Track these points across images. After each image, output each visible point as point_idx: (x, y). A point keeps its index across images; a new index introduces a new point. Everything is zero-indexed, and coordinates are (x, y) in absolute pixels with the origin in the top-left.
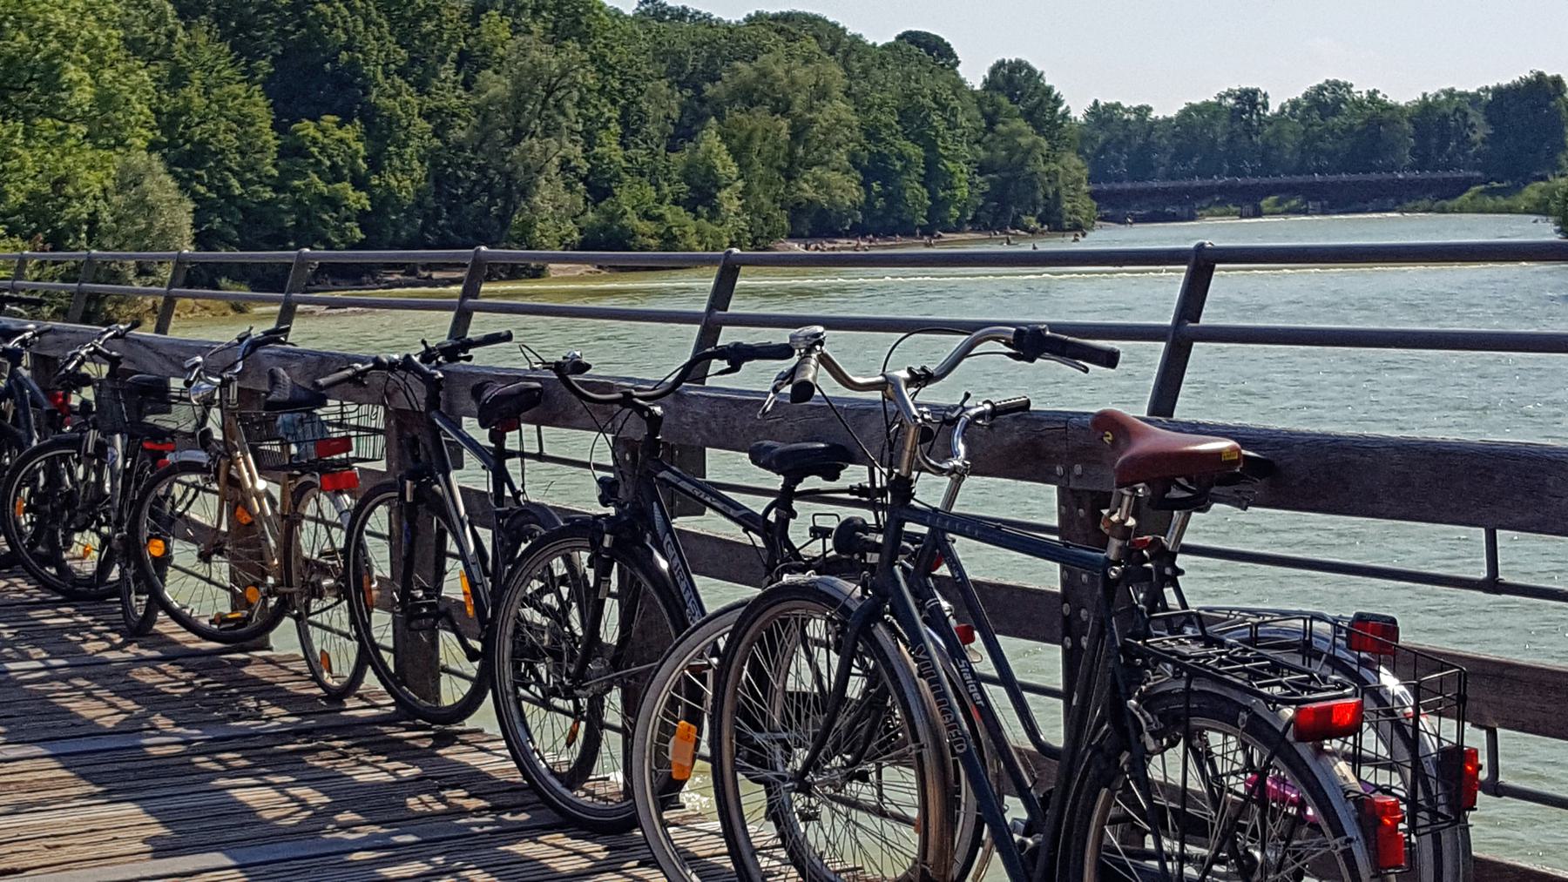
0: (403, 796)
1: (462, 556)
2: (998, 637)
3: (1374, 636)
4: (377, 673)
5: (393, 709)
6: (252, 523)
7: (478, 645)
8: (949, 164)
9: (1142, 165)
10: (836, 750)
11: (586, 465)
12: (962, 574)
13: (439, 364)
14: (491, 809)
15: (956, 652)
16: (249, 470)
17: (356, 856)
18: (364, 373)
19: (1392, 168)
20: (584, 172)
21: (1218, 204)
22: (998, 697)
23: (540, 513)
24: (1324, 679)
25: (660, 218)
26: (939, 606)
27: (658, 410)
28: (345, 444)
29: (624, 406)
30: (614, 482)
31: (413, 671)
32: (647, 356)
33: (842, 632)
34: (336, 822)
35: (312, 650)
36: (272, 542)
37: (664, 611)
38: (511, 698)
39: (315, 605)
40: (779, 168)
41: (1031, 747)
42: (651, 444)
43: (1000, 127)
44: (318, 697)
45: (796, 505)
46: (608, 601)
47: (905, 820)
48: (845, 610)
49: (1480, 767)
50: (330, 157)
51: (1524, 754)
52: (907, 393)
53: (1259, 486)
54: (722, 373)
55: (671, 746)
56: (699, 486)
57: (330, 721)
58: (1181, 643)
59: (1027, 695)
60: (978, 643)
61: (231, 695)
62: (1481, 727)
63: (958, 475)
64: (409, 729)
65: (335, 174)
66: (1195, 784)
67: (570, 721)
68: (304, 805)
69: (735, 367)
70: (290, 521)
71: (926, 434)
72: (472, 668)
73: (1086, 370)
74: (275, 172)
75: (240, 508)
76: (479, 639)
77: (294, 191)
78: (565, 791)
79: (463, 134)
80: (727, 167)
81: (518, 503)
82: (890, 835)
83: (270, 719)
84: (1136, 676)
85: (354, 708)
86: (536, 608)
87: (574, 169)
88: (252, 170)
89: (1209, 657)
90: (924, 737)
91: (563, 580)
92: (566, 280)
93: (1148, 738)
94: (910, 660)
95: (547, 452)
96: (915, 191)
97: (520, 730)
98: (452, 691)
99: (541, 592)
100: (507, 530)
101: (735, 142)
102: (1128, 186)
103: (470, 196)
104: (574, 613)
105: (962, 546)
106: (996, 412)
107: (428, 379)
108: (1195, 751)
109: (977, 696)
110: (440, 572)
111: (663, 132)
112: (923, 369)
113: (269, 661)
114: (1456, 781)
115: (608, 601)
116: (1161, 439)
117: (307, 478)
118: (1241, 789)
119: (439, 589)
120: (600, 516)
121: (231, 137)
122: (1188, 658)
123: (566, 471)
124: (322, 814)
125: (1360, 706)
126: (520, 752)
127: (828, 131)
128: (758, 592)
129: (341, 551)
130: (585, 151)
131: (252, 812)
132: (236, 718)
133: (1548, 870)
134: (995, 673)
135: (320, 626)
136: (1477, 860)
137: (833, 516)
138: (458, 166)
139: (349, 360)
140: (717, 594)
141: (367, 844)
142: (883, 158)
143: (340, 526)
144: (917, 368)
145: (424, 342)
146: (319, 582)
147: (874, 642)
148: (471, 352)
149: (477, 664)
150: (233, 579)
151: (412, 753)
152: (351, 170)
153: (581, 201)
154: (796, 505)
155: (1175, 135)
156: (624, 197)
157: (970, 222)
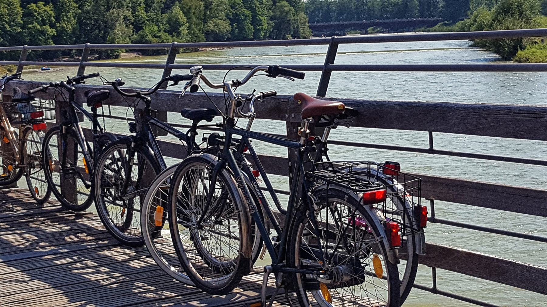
0: (64, 236)
1: (83, 152)
2: (267, 174)
3: (392, 169)
4: (55, 194)
5: (61, 206)
6: (9, 143)
7: (90, 183)
8: (261, 17)
9: (327, 15)
10: (211, 215)
11: (125, 119)
12: (254, 152)
13: (73, 84)
14: (95, 240)
15: (252, 179)
16: (8, 124)
17: (46, 257)
18: (46, 88)
19: (412, 17)
20: (132, 21)
21: (353, 30)
22: (267, 195)
23: (109, 136)
24: (373, 183)
25: (159, 37)
26: (246, 164)
27: (149, 98)
28: (41, 114)
29: (137, 98)
30: (135, 124)
31: (68, 193)
32: (144, 78)
33: (211, 173)
34: (39, 246)
35: (32, 186)
36: (17, 150)
37: (154, 170)
38: (100, 200)
39: (33, 171)
40: (201, 19)
41: (279, 212)
42: (147, 111)
43: (277, 4)
44: (34, 203)
45: (197, 130)
46: (134, 166)
47: (236, 238)
48: (213, 165)
49: (427, 213)
50: (41, 16)
51: (444, 208)
52: (232, 89)
53: (353, 119)
54: (172, 85)
55: (155, 214)
56: (164, 125)
57: (37, 211)
58: (326, 173)
59: (266, 187)
60: (260, 177)
61: (3, 203)
62: (429, 200)
63: (251, 118)
64: (66, 213)
65: (43, 23)
66: (331, 221)
67: (122, 208)
68: (28, 240)
69: (176, 83)
70: (22, 142)
71: (239, 104)
72: (88, 192)
73: (294, 80)
74: (22, 22)
75: (5, 138)
76: (90, 181)
77: (29, 29)
78: (121, 233)
79: (89, 8)
80: (182, 18)
81: (102, 133)
82: (232, 244)
83: (17, 211)
84: (310, 184)
85: (47, 206)
86: (109, 169)
87: (129, 20)
88: (13, 21)
89: (334, 177)
90: (240, 208)
91: (118, 160)
92: (126, 58)
93: (315, 205)
94: (235, 182)
95: (112, 115)
96: (249, 27)
97: (104, 212)
98: (81, 200)
99: (111, 164)
100: (98, 142)
101: (185, 10)
102: (322, 24)
103: (92, 30)
104: (123, 171)
105: (255, 143)
106: (264, 96)
107: (69, 90)
108: (331, 210)
109: (259, 194)
110: (76, 158)
111: (160, 6)
112: (237, 80)
113: (17, 191)
114: (419, 218)
115: (134, 166)
116: (321, 102)
117: (28, 126)
118: (347, 222)
119: (76, 164)
120: (130, 136)
121: (5, 9)
122: (328, 177)
123: (118, 121)
124: (35, 243)
125: (385, 192)
126: (104, 220)
127: (218, 6)
128: (182, 161)
129: (41, 152)
130: (132, 13)
131: (9, 243)
132: (5, 211)
133: (451, 247)
134: (266, 187)
135: (34, 178)
136: (427, 245)
137: (207, 134)
138: (88, 19)
139: (41, 84)
140: (170, 161)
141: (50, 253)
142: (237, 15)
143: (40, 143)
144: (235, 80)
145: (68, 77)
146: (33, 162)
147: (222, 176)
148: (85, 80)
149: (90, 190)
150: (3, 163)
151: (67, 222)
152: (49, 21)
153: (131, 31)
154: (198, 130)
155: (339, 6)
156: (147, 30)
157: (268, 37)
